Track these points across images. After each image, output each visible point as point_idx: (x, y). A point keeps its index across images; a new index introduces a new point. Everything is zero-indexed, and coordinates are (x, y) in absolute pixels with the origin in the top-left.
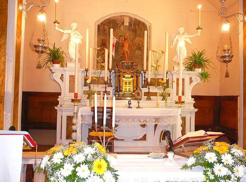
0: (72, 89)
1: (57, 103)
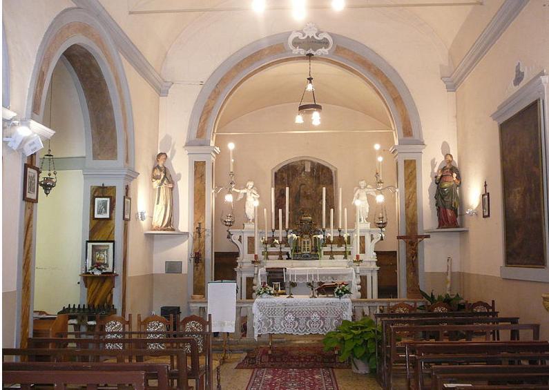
0: (251, 250)
1: (236, 265)
